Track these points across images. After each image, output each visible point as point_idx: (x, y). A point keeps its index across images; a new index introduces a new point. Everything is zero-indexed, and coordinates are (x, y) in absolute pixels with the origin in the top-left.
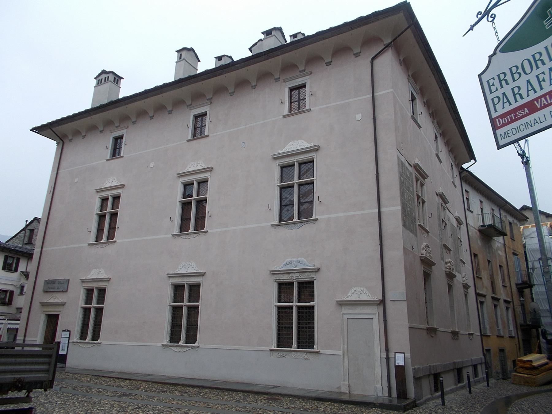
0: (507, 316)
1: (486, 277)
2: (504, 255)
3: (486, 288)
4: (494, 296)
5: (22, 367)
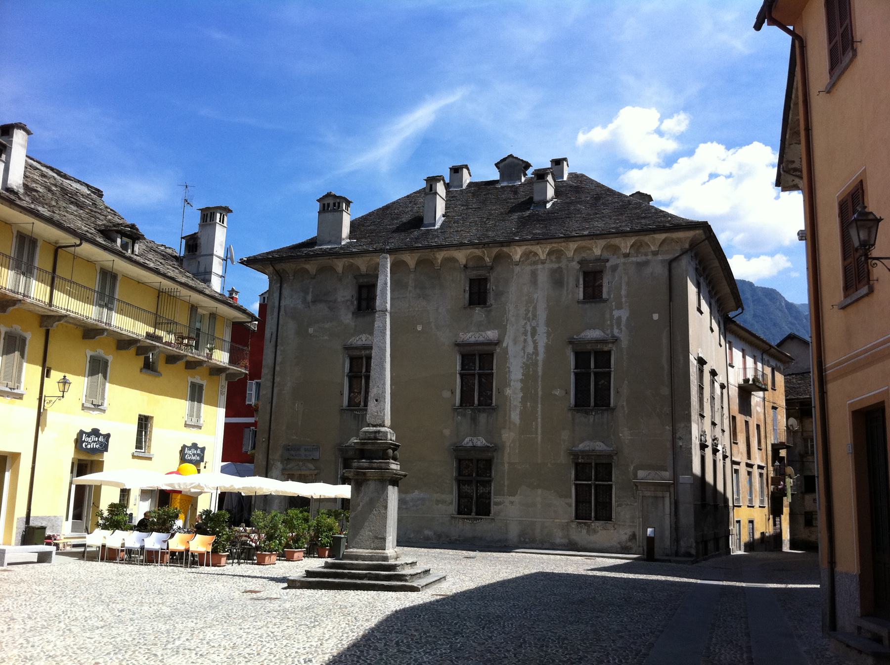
0: (815, 402)
1: (742, 441)
2: (763, 411)
3: (742, 454)
4: (749, 461)
5: (359, 582)
